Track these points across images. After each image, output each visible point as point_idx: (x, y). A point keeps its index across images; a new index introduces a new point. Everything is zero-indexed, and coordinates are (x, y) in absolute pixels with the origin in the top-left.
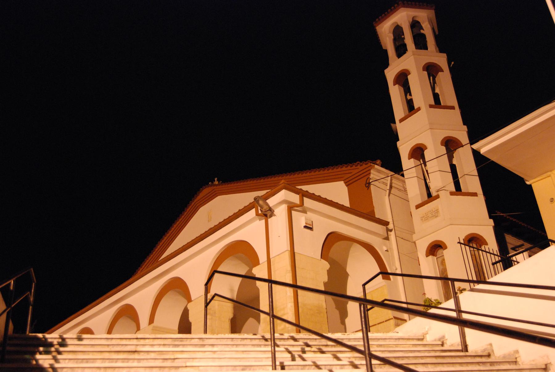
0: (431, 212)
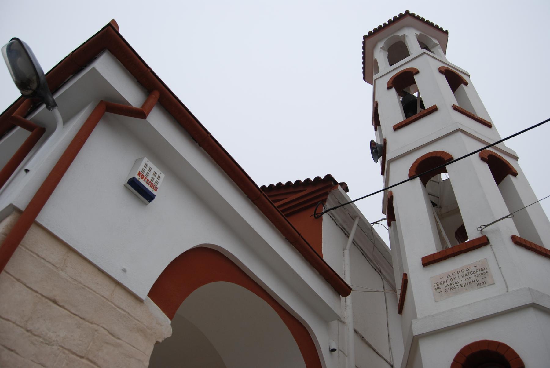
0: (465, 272)
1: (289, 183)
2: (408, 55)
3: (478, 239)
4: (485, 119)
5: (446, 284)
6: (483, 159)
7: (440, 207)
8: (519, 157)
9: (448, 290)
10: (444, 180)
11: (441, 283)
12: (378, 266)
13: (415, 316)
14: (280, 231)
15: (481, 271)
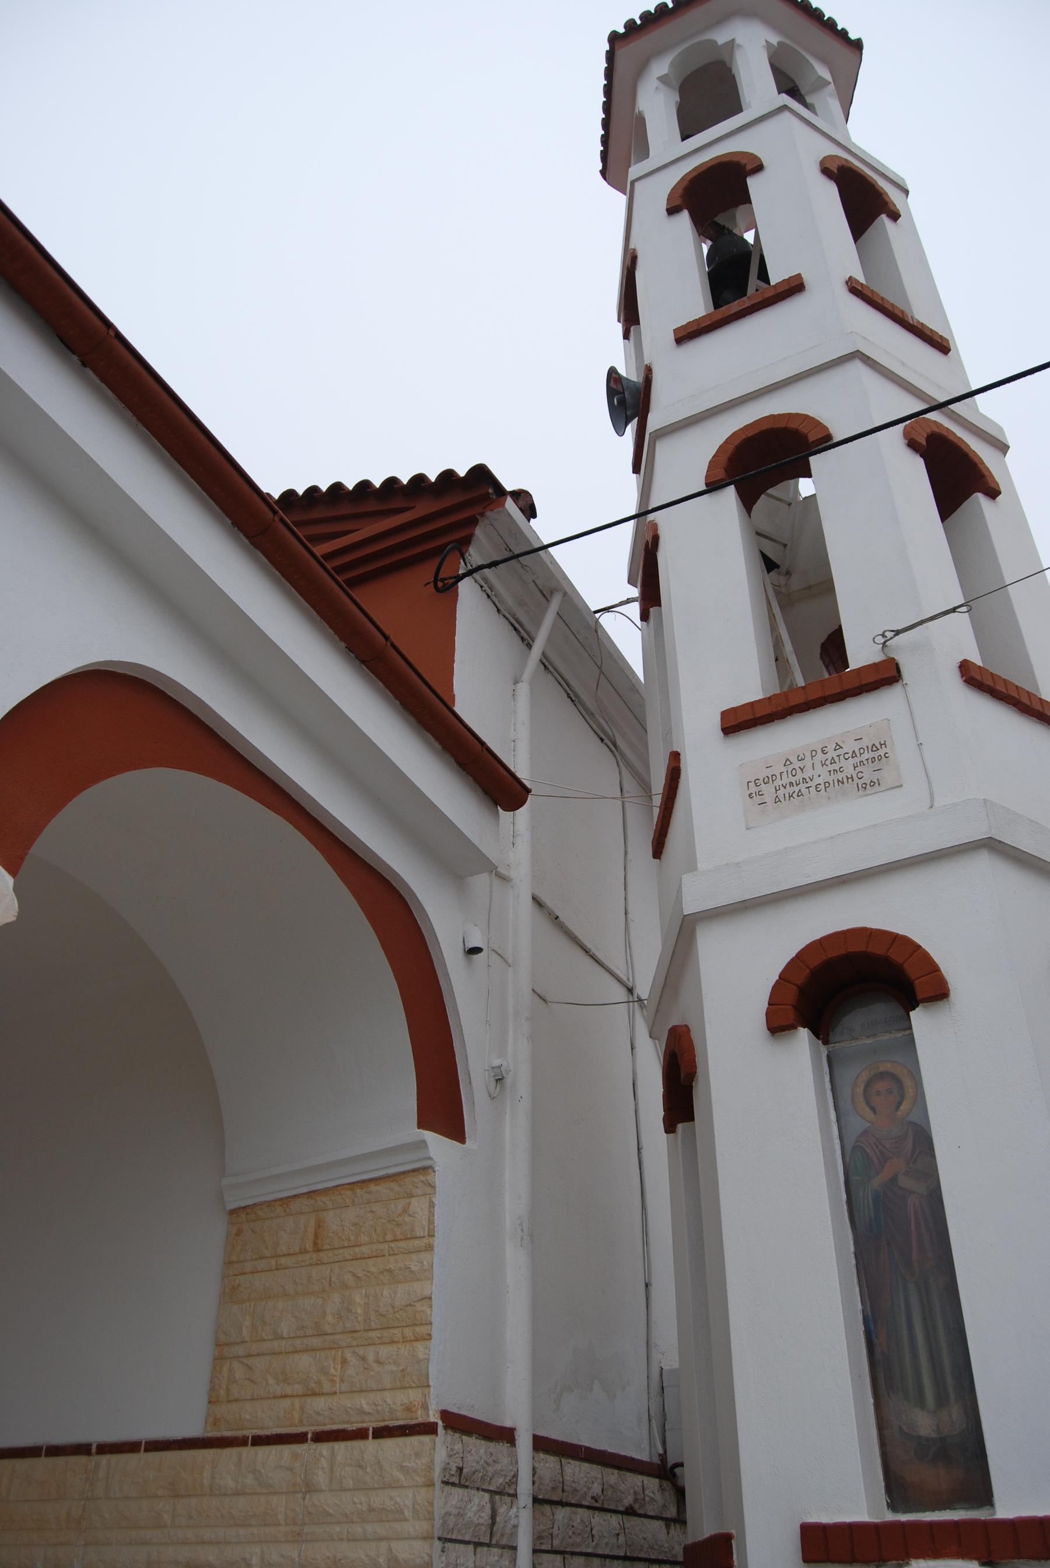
0: (832, 754)
1: (364, 486)
2: (735, 107)
3: (874, 667)
4: (933, 328)
5: (778, 782)
6: (912, 445)
7: (788, 573)
8: (1010, 444)
9: (782, 799)
10: (806, 498)
11: (766, 779)
12: (610, 728)
13: (692, 867)
14: (331, 626)
15: (872, 751)
